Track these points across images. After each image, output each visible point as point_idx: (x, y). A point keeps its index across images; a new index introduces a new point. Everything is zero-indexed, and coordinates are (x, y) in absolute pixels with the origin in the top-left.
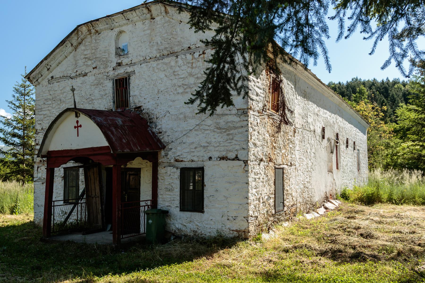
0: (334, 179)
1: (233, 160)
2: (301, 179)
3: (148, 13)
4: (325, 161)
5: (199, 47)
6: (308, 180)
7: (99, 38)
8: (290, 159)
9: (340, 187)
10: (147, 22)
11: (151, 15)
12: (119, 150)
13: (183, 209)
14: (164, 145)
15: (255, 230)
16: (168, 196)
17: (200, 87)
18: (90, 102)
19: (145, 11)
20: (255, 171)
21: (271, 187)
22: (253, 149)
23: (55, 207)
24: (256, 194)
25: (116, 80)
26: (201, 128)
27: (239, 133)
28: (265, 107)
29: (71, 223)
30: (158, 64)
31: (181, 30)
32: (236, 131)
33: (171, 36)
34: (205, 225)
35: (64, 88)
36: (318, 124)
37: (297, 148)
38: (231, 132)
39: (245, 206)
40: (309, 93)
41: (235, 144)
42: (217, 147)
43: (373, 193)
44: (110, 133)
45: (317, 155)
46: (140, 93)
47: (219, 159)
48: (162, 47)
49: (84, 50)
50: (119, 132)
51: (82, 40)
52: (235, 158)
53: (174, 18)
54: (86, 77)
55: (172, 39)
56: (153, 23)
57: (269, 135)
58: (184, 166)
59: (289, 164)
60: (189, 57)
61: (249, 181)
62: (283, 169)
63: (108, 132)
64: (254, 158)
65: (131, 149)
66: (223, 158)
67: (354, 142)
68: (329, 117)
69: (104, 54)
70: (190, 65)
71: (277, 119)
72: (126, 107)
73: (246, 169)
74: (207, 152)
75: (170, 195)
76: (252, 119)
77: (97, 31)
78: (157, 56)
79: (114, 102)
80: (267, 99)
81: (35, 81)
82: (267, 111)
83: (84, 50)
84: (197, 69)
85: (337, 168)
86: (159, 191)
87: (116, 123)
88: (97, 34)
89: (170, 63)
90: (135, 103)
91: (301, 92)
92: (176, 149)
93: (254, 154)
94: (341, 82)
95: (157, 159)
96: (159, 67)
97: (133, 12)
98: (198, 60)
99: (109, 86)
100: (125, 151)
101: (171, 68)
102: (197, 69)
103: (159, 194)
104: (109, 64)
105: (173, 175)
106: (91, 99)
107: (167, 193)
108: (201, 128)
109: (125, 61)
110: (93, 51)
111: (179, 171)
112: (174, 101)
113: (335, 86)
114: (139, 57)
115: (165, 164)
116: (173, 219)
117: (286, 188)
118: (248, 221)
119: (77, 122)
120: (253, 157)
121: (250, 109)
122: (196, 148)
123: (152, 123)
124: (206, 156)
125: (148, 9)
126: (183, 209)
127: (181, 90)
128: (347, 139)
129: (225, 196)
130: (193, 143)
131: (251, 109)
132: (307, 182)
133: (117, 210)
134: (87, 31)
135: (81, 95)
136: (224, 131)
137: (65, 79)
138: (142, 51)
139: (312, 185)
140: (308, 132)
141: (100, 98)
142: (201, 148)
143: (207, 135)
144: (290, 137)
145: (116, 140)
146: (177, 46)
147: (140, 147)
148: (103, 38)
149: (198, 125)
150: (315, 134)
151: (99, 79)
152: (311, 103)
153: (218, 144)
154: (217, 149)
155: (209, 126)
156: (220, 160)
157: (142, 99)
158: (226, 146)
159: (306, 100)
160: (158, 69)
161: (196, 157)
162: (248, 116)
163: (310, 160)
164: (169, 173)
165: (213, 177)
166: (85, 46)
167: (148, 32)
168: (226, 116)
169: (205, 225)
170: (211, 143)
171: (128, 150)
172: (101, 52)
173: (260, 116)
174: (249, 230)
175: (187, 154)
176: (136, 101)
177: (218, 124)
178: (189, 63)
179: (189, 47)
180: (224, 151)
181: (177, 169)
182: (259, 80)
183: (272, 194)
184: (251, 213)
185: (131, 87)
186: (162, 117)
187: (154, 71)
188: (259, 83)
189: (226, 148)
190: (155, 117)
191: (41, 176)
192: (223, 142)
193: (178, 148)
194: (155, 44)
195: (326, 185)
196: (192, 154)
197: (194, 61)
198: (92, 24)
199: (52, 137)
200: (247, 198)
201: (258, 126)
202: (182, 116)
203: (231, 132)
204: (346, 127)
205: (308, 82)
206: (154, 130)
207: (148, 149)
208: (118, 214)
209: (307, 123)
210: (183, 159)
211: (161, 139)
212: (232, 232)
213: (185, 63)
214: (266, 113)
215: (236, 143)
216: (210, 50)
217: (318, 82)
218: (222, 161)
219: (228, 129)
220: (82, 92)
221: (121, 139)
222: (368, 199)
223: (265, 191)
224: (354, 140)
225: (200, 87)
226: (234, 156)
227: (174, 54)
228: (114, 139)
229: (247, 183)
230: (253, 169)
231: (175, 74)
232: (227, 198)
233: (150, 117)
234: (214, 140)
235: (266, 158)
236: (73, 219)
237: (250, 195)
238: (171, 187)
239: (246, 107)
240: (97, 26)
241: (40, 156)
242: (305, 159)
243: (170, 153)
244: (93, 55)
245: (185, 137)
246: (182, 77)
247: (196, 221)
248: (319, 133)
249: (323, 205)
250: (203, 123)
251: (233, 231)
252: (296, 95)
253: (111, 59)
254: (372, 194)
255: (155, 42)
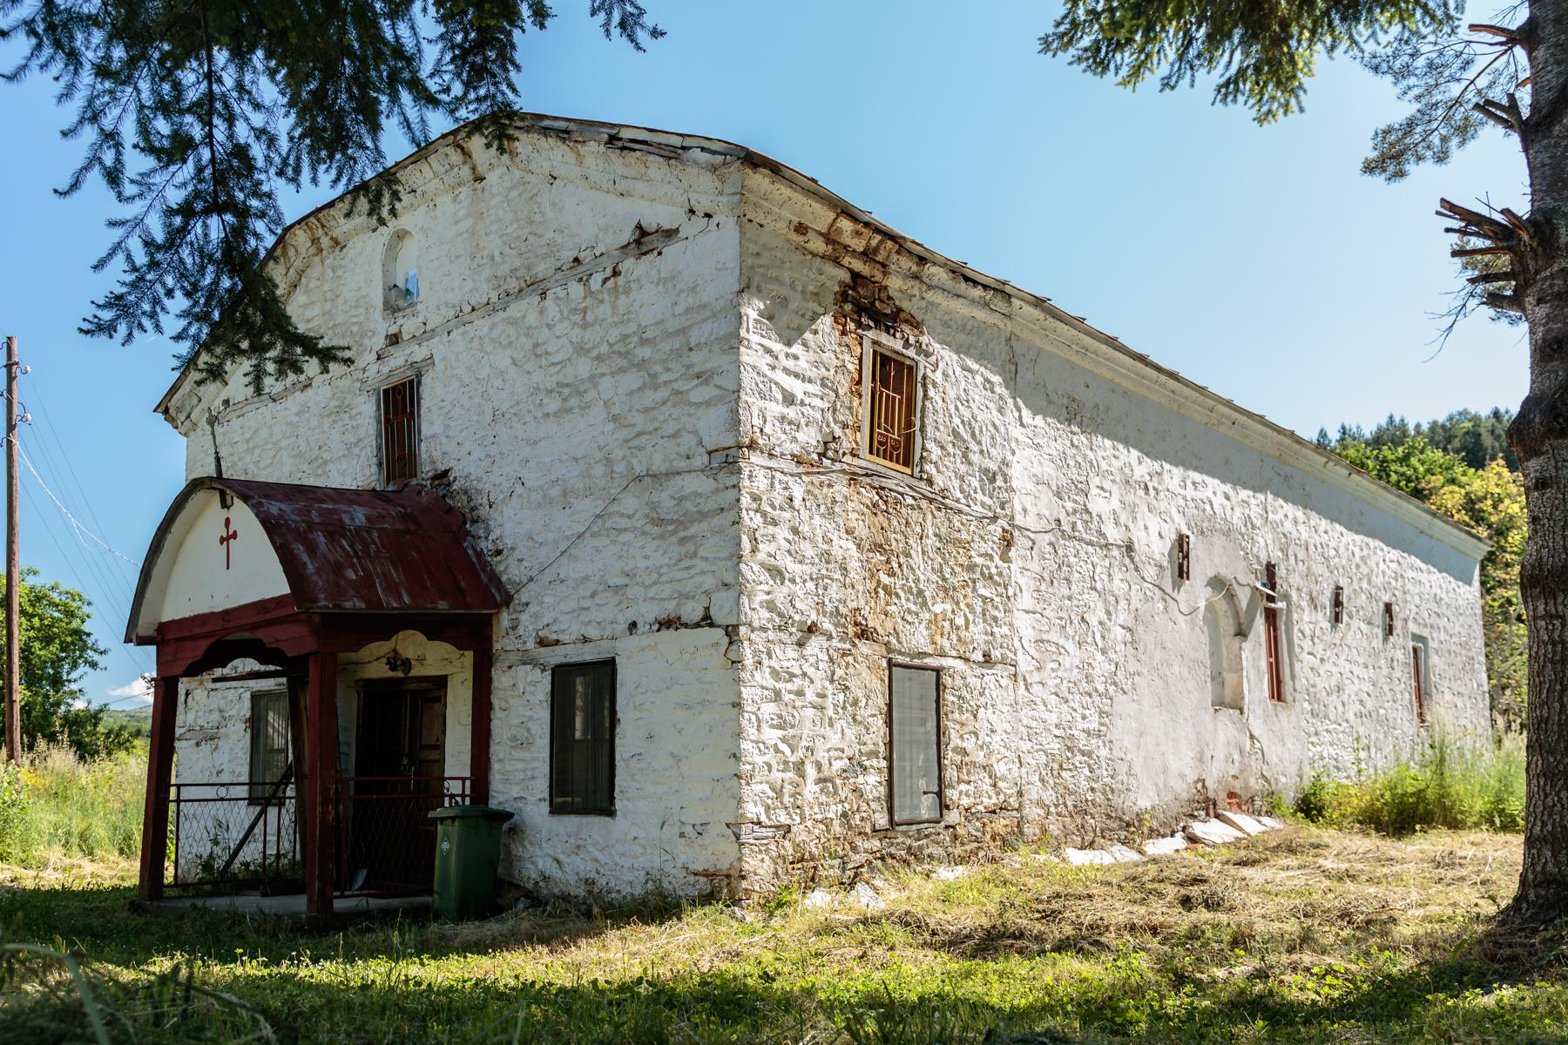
0: (1252, 737)
1: (697, 625)
2: (1053, 718)
3: (465, 162)
4: (1195, 661)
5: (602, 254)
6: (1095, 726)
7: (343, 263)
8: (981, 638)
9: (1293, 770)
10: (465, 191)
11: (474, 169)
12: (323, 603)
13: (556, 810)
14: (506, 592)
15: (776, 873)
16: (520, 766)
17: (124, 284)
18: (320, 471)
19: (456, 156)
20: (774, 663)
21: (867, 729)
22: (765, 588)
23: (182, 804)
24: (783, 747)
25: (386, 392)
26: (609, 524)
27: (713, 533)
28: (833, 445)
29: (247, 865)
30: (494, 325)
31: (554, 204)
32: (705, 525)
33: (529, 230)
34: (617, 858)
35: (254, 433)
36: (1154, 524)
37: (1026, 601)
38: (692, 531)
39: (729, 784)
40: (1097, 406)
41: (703, 573)
42: (651, 586)
43: (1420, 791)
44: (300, 549)
45: (1147, 638)
46: (447, 426)
47: (656, 627)
48: (504, 270)
49: (305, 306)
50: (342, 547)
51: (300, 273)
52: (703, 620)
53: (533, 166)
54: (309, 392)
55: (531, 238)
56: (479, 193)
57: (859, 546)
58: (563, 660)
59: (978, 656)
60: (576, 290)
61: (744, 696)
62: (938, 671)
63: (293, 546)
64: (771, 620)
65: (373, 601)
66: (667, 624)
67: (1388, 608)
68: (1218, 501)
69: (353, 312)
70: (578, 318)
71: (901, 489)
72: (411, 477)
73: (732, 655)
74: (624, 605)
75: (524, 760)
76: (761, 482)
77: (336, 242)
78: (492, 301)
79: (380, 464)
80: (841, 418)
81: (183, 419)
82: (848, 459)
83: (305, 306)
84: (597, 327)
85: (1277, 693)
86: (494, 748)
87: (341, 521)
88: (338, 248)
89: (524, 317)
90: (433, 463)
91: (1050, 402)
92: (541, 603)
93: (770, 606)
94: (1502, 410)
95: (488, 640)
96: (495, 334)
97: (423, 165)
98: (600, 297)
99: (367, 412)
100: (348, 604)
101: (527, 335)
102: (597, 327)
103: (493, 759)
104: (367, 342)
105: (532, 693)
106: (320, 461)
107: (516, 754)
108: (609, 524)
109: (409, 326)
110: (328, 305)
111: (548, 675)
112: (535, 443)
113: (1477, 425)
114: (443, 310)
115: (513, 657)
116: (531, 843)
117: (955, 741)
118: (738, 837)
119: (228, 522)
120: (765, 614)
121: (750, 447)
122: (593, 595)
123: (477, 521)
124: (621, 619)
125: (462, 149)
126: (556, 810)
127: (553, 405)
128: (1339, 588)
129: (672, 755)
130: (586, 578)
131: (752, 446)
132: (1088, 732)
133: (319, 799)
134: (309, 244)
135: (296, 452)
136: (670, 528)
137: (257, 405)
138: (453, 290)
139: (1116, 745)
140: (1090, 549)
141: (344, 456)
142: (609, 594)
143: (625, 548)
144: (979, 561)
145: (318, 571)
146: (545, 257)
147: (411, 595)
148: (351, 260)
149: (599, 516)
150: (1132, 559)
151: (343, 392)
152: (1108, 443)
153: (655, 576)
154: (651, 593)
155: (629, 517)
156: (659, 630)
157: (450, 447)
158: (678, 581)
159: (1075, 429)
160: (493, 340)
161: (594, 624)
162: (739, 471)
163: (1103, 652)
164: (521, 686)
165: (640, 690)
166: (307, 292)
167: (468, 223)
168: (678, 477)
169: (617, 858)
170: (635, 575)
171: (358, 604)
172: (347, 308)
173: (807, 473)
174: (741, 871)
175: (569, 616)
176: (437, 455)
177: (653, 506)
178: (574, 311)
179: (576, 260)
180: (671, 598)
181: (543, 671)
182: (797, 349)
183: (873, 754)
184: (752, 810)
185: (422, 410)
186: (503, 501)
187: (481, 349)
188: (796, 358)
189: (678, 586)
190: (485, 501)
191: (195, 721)
192: (669, 566)
193: (546, 599)
194: (485, 261)
195: (1202, 753)
196: (584, 617)
197: (589, 301)
198: (318, 220)
199: (168, 577)
200: (735, 755)
201: (792, 507)
202: (555, 492)
203: (692, 531)
204: (1333, 544)
205: (1085, 364)
206: (483, 545)
207: (442, 605)
208: (324, 813)
209: (1086, 517)
210: (561, 637)
211: (501, 572)
212: (692, 879)
213: (566, 313)
214: (838, 466)
215: (706, 567)
216: (632, 260)
217: (1140, 366)
218: (665, 633)
219: (682, 522)
220: (301, 441)
221: (338, 569)
222: (1400, 813)
223: (834, 739)
224: (1386, 598)
225: (124, 284)
226: (697, 615)
227: (536, 287)
228: (310, 566)
229: (737, 705)
230: (764, 656)
231: (540, 351)
232: (679, 760)
233: (472, 504)
234: (643, 564)
235: (836, 626)
236: (251, 853)
237: (745, 745)
238: (526, 734)
239: (731, 443)
240: (333, 223)
241: (134, 637)
242: (1070, 646)
243: (524, 617)
244: (327, 317)
245: (564, 559)
246: (556, 360)
247: (594, 845)
248: (1157, 557)
249: (1184, 830)
250: (615, 507)
251: (696, 874)
252: (1019, 410)
253: (371, 326)
254: (1419, 794)
255: (486, 252)
